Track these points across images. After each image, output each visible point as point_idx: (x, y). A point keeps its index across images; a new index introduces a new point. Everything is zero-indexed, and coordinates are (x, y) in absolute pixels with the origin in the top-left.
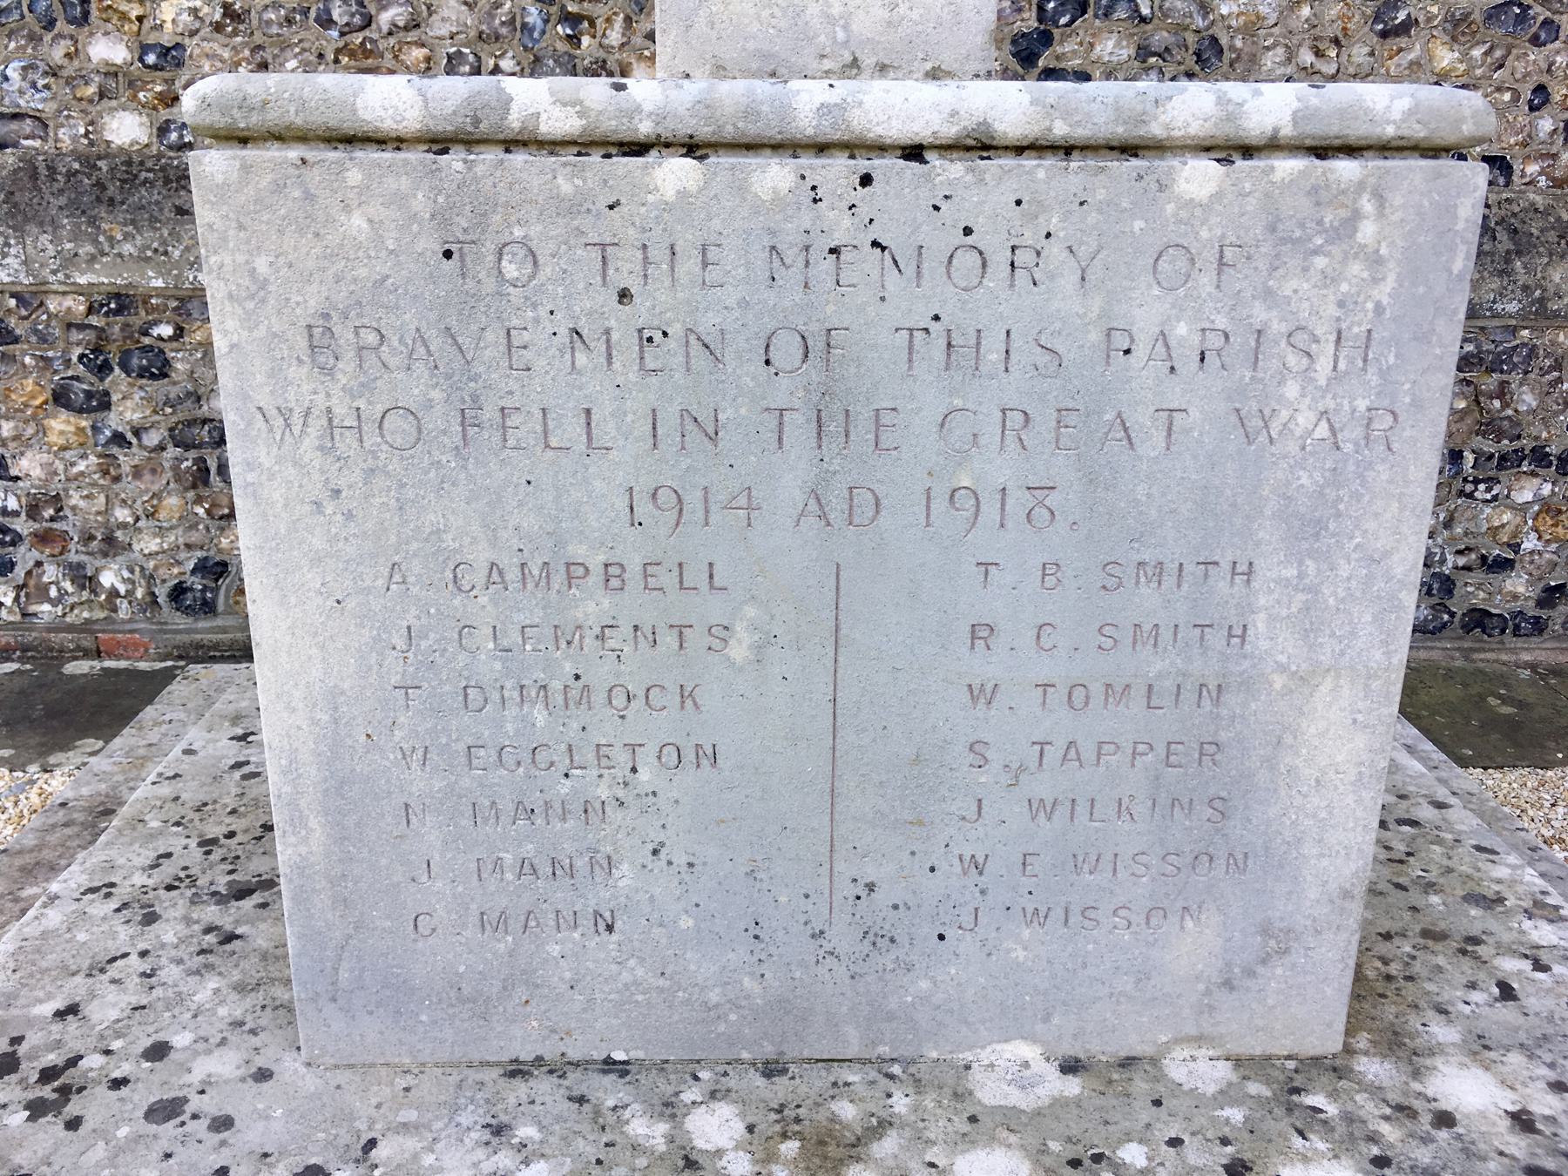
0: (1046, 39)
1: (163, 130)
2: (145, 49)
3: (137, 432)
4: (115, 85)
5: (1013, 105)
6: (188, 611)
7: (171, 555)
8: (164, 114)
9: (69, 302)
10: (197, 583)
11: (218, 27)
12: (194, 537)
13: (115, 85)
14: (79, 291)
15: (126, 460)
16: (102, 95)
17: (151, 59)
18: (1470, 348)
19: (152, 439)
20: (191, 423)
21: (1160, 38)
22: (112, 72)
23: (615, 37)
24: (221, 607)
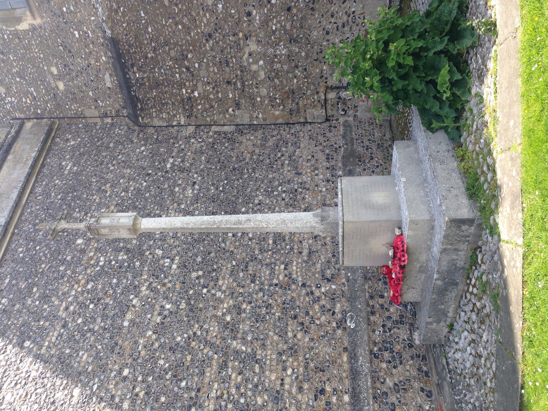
0: (327, 279)
1: (346, 393)
2: (334, 394)
3: (398, 399)
4: (340, 399)
5: (340, 208)
6: (432, 395)
7: (421, 397)
8: (344, 392)
9: (376, 406)
10: (425, 392)
11: (330, 382)
12: (416, 392)
13: (340, 399)
14: (373, 404)
15: (403, 401)
16: (341, 401)
17: (335, 393)
18: (223, 213)
19: (399, 396)
20: (395, 390)
21: (327, 267)
22: (337, 399)
23: (329, 328)
24: (430, 389)
